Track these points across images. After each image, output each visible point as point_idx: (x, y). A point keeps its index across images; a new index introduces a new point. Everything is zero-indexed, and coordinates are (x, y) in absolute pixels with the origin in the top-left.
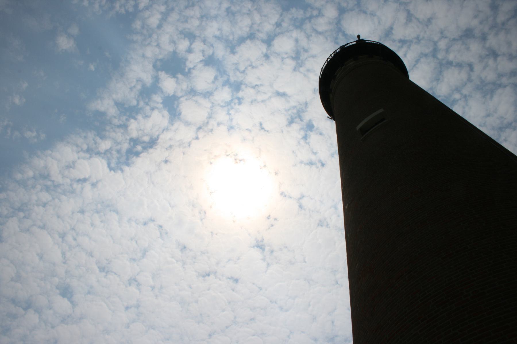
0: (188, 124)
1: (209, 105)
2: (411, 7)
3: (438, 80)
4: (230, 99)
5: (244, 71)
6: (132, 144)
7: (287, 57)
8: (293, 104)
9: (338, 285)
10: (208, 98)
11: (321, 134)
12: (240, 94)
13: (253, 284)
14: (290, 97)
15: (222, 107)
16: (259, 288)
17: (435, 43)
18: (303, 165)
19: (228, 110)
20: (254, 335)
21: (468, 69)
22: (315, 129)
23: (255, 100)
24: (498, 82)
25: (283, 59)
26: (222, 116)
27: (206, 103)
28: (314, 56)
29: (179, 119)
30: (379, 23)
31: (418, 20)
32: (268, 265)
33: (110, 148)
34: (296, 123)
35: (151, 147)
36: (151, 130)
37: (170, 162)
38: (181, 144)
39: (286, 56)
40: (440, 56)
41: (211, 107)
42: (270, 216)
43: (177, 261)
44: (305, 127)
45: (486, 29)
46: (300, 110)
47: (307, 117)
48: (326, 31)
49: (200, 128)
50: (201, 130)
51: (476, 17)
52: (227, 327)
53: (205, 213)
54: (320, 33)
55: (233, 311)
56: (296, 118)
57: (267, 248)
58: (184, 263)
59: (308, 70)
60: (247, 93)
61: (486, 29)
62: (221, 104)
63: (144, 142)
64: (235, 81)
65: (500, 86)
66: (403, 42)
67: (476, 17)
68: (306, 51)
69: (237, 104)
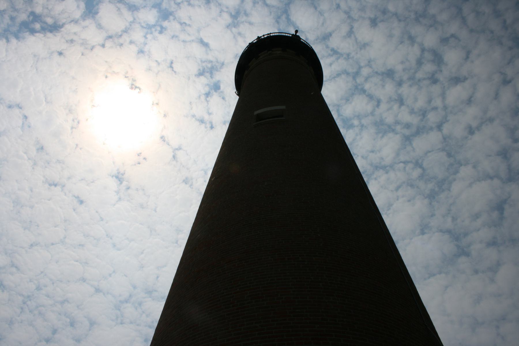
0: (100, 27)
1: (131, 19)
2: (356, 25)
3: (347, 100)
4: (153, 24)
5: (179, 3)
6: (31, 18)
7: (227, 12)
8: (210, 57)
9: (176, 244)
10: (133, 11)
11: (223, 98)
12: (165, 24)
13: (97, 212)
14: (210, 50)
15: (142, 27)
16: (101, 218)
17: (360, 68)
18: (194, 119)
19: (147, 34)
20: (77, 261)
21: (376, 103)
22: (219, 91)
23: (177, 37)
24: (393, 127)
25: (222, 11)
26: (138, 35)
27: (128, 16)
28: (251, 24)
29: (93, 17)
30: (323, 24)
31: (356, 39)
32: (120, 199)
33: (4, 11)
34: (205, 77)
35: (51, 31)
36: (59, 14)
37: (64, 56)
38: (84, 43)
39: (225, 10)
40: (359, 80)
41: (131, 22)
42: (141, 153)
43: (29, 159)
44: (212, 84)
45: (405, 78)
46: (215, 67)
47: (218, 77)
48: (273, 6)
49: (110, 37)
50: (111, 40)
51: (402, 63)
52: (52, 244)
53: (79, 123)
54: (267, 5)
55: (65, 230)
56: (207, 72)
57: (125, 183)
58: (35, 164)
59: (240, 34)
60: (172, 25)
61: (405, 78)
62: (143, 24)
63: (45, 23)
64: (166, 9)
65: (393, 131)
66: (335, 52)
67: (402, 63)
68: (246, 14)
69: (157, 32)
